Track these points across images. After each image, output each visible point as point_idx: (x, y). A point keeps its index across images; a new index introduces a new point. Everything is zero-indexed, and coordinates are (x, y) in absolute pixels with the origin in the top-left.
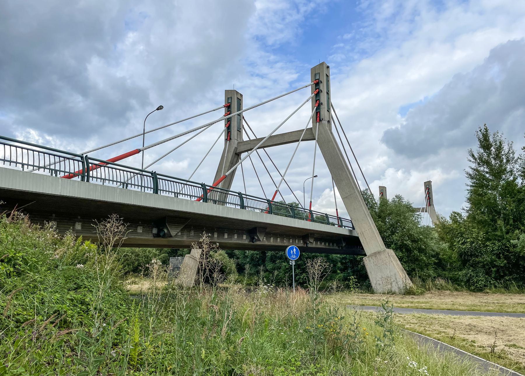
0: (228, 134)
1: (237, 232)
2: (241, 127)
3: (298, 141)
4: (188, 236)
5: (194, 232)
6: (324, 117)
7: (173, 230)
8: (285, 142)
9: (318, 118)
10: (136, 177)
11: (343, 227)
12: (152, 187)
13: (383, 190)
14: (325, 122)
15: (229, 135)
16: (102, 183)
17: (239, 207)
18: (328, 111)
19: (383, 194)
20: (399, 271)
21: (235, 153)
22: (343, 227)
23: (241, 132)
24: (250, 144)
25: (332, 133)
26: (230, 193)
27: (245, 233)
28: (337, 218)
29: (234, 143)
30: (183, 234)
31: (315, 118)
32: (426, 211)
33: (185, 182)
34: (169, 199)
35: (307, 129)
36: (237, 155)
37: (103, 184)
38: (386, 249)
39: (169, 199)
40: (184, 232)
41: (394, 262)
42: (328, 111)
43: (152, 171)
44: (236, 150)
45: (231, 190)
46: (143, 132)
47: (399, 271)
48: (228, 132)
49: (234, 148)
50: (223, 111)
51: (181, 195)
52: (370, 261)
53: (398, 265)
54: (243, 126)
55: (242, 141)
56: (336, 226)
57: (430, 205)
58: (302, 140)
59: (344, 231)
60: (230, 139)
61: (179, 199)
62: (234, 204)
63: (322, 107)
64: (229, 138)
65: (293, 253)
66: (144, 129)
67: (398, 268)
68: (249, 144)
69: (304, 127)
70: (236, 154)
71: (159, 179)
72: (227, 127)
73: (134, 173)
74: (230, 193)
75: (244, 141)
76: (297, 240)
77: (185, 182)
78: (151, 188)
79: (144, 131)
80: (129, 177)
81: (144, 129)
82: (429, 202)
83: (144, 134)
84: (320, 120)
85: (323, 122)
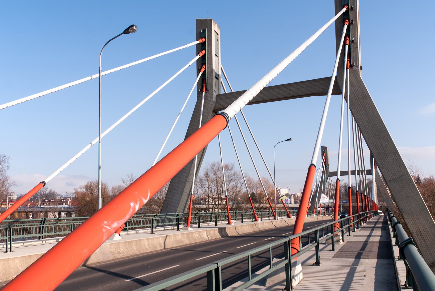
21: (213, 110)
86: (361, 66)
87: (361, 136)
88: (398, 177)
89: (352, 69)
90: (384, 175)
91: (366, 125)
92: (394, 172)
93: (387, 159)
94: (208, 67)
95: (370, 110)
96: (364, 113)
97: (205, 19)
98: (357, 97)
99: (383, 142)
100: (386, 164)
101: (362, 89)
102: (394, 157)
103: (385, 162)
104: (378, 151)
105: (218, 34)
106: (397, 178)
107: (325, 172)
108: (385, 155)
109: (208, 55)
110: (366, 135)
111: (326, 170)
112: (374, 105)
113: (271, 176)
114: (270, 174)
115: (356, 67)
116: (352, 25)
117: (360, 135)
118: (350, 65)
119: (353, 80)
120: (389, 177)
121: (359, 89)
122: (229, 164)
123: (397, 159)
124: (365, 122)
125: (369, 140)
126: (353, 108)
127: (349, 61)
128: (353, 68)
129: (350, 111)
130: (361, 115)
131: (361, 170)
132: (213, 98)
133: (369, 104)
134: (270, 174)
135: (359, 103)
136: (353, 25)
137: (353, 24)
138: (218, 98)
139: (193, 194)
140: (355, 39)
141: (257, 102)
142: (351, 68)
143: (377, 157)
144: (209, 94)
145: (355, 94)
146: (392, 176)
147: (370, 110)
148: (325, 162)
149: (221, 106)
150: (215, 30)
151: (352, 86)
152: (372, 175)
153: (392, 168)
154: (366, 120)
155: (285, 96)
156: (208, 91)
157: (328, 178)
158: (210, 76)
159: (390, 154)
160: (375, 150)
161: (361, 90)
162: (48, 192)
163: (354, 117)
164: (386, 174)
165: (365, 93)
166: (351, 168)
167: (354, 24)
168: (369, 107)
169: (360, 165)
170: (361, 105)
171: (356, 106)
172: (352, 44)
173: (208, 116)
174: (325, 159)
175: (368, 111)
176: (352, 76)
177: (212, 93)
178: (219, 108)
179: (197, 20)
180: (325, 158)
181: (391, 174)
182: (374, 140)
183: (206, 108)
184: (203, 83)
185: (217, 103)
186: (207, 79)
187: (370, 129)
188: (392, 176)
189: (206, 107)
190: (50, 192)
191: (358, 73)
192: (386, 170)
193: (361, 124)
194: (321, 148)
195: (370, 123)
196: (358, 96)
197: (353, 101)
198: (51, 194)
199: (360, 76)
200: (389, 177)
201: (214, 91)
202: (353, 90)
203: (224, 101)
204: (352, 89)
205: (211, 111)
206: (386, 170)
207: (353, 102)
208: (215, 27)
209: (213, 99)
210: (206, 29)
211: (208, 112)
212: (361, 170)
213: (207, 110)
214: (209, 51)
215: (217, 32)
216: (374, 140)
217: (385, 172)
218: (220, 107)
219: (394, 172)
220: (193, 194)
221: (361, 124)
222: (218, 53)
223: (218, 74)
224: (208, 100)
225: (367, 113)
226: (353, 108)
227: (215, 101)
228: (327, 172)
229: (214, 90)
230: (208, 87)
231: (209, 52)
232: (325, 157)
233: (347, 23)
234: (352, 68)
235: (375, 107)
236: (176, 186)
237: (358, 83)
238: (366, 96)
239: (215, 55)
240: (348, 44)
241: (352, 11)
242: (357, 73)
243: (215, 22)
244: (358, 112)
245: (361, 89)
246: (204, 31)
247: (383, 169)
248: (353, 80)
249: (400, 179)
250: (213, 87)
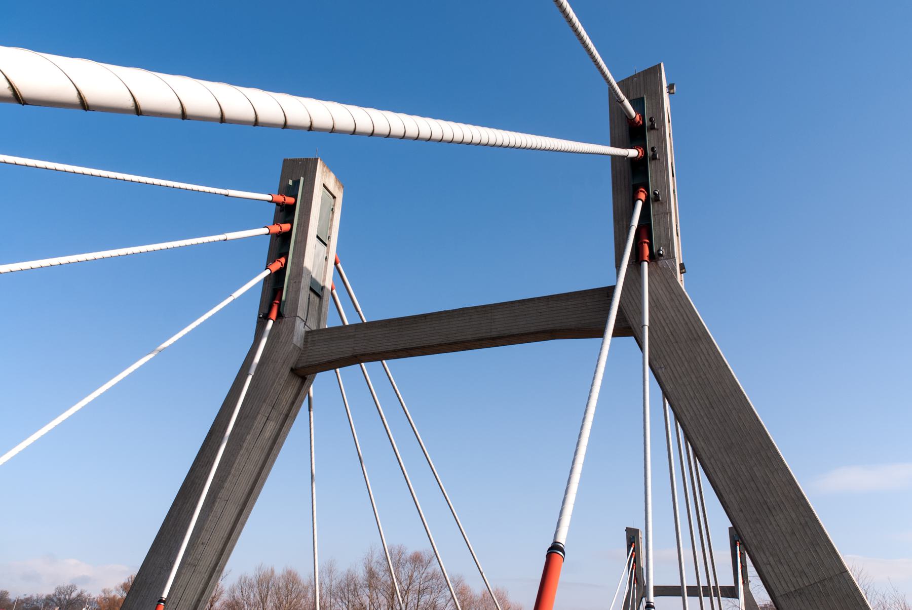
8: (494, 334)
21: (292, 370)
86: (683, 263)
87: (697, 470)
88: (812, 582)
89: (657, 264)
90: (765, 574)
91: (702, 415)
92: (798, 566)
93: (773, 523)
94: (292, 263)
95: (710, 374)
96: (694, 380)
97: (304, 159)
98: (671, 337)
99: (755, 469)
100: (770, 536)
101: (685, 316)
102: (794, 516)
103: (766, 530)
104: (740, 494)
105: (334, 197)
106: (815, 585)
107: (635, 585)
108: (765, 507)
109: (299, 235)
110: (703, 444)
111: (637, 582)
112: (723, 361)
113: (483, 577)
114: (481, 572)
115: (667, 259)
116: (653, 162)
117: (695, 462)
118: (650, 254)
119: (660, 291)
120: (783, 583)
121: (676, 315)
122: (424, 553)
123: (803, 522)
124: (699, 407)
125: (712, 460)
126: (662, 366)
127: (647, 243)
128: (660, 263)
129: (649, 373)
130: (685, 386)
131: (714, 585)
132: (293, 336)
133: (707, 356)
134: (482, 571)
135: (680, 352)
136: (656, 161)
137: (656, 158)
138: (309, 340)
139: (164, 602)
140: (661, 191)
141: (407, 349)
142: (654, 263)
143: (741, 514)
144: (285, 326)
145: (666, 330)
146: (794, 580)
147: (710, 374)
148: (634, 562)
149: (315, 359)
150: (324, 184)
151: (657, 308)
152: (738, 599)
153: (791, 554)
154: (701, 402)
155: (478, 336)
156: (284, 320)
157: (642, 598)
158: (295, 282)
159: (782, 506)
160: (734, 492)
161: (684, 319)
162: (74, 595)
163: (680, 424)
164: (773, 571)
165: (695, 326)
166: (690, 581)
167: (659, 159)
168: (706, 363)
169: (709, 568)
170: (683, 359)
171: (668, 360)
172: (656, 204)
173: (273, 383)
174: (634, 556)
175: (705, 375)
176: (655, 282)
177: (293, 324)
178: (308, 363)
179: (285, 160)
180: (634, 553)
181: (790, 573)
182: (728, 460)
183: (272, 362)
184: (274, 298)
185: (306, 350)
186: (287, 291)
187: (715, 428)
188: (794, 580)
189: (272, 358)
190: (79, 596)
191: (672, 275)
192: (771, 559)
193: (686, 413)
194: (626, 530)
195: (711, 410)
196: (674, 334)
197: (662, 348)
198: (80, 601)
199: (677, 282)
200: (783, 583)
201: (298, 321)
202: (661, 318)
203: (323, 346)
204: (659, 314)
205: (286, 372)
206: (771, 559)
207: (661, 351)
208: (324, 178)
209: (292, 338)
210: (302, 179)
211: (277, 372)
212: (714, 585)
213: (274, 367)
214: (302, 225)
215: (332, 192)
216: (728, 460)
217: (770, 564)
218: (310, 362)
219: (798, 566)
220: (164, 602)
221: (687, 410)
222: (329, 239)
223: (322, 284)
224: (280, 340)
225: (703, 380)
226: (662, 366)
227: (298, 345)
228: (641, 586)
229: (299, 317)
230: (286, 311)
231: (302, 228)
232: (634, 550)
233: (738, 545)
234: (656, 261)
235: (726, 366)
236: (156, 575)
237: (672, 299)
238: (698, 334)
239: (318, 237)
240: (644, 200)
241: (652, 132)
242: (670, 274)
243: (331, 167)
244: (675, 377)
245: (682, 316)
246: (297, 183)
247: (762, 555)
248: (660, 291)
249: (820, 592)
250: (297, 309)
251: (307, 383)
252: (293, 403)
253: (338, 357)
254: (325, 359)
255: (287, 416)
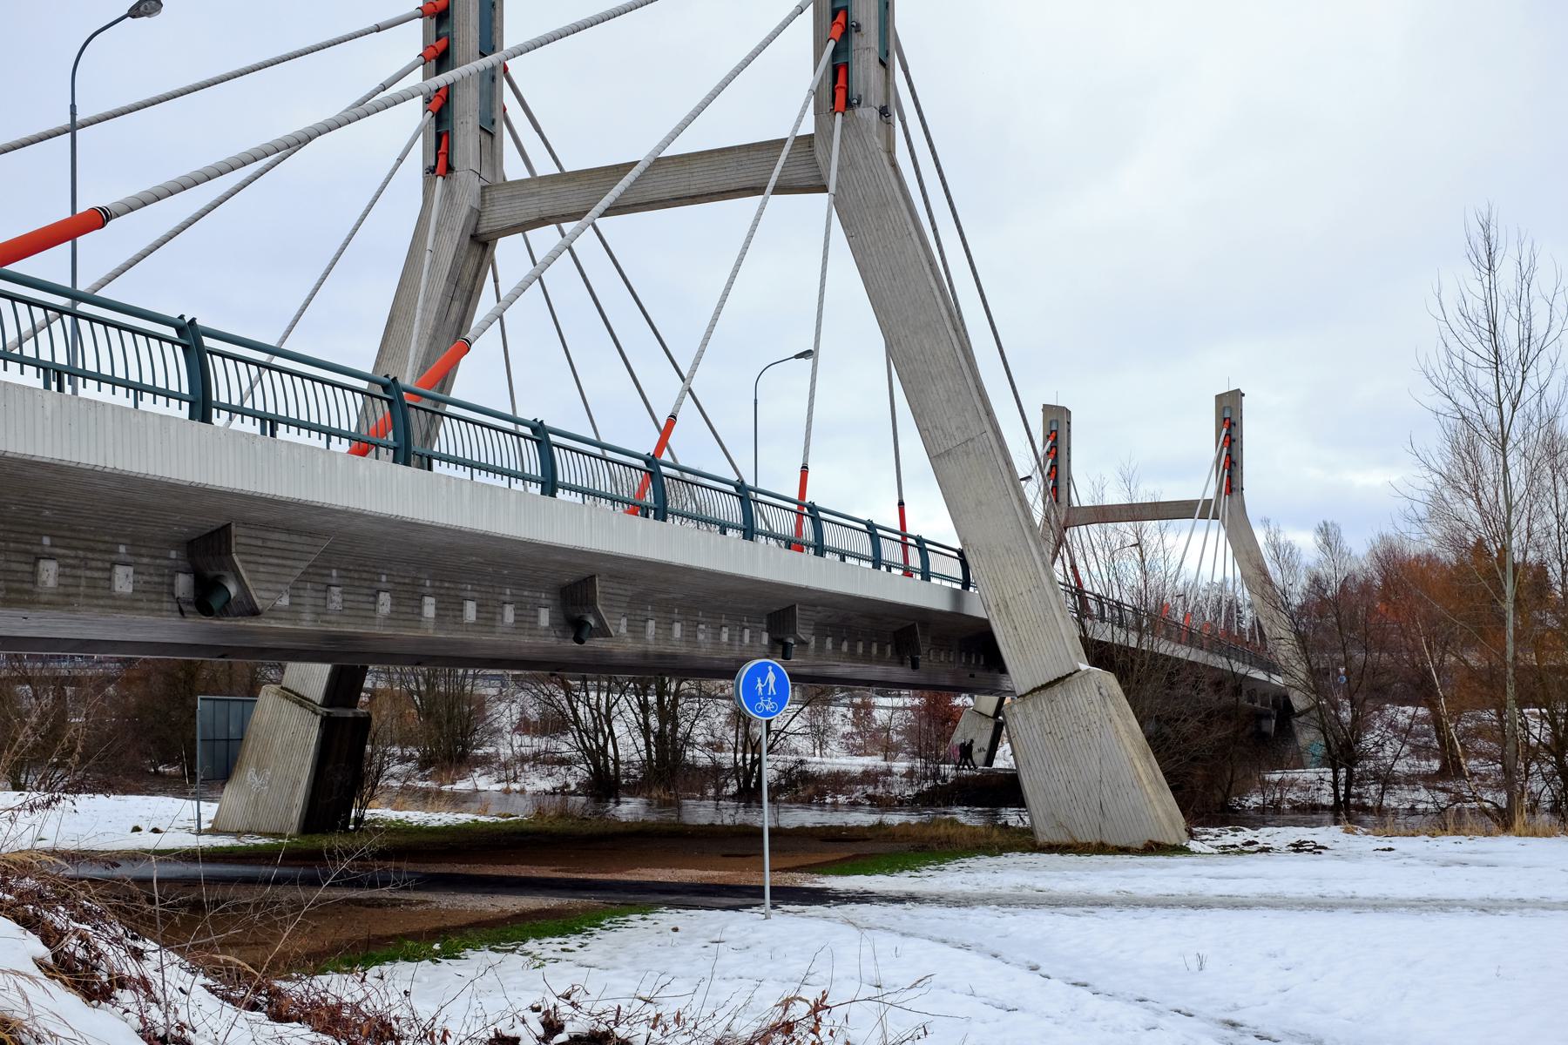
0: (438, 147)
1: (512, 595)
2: (498, 115)
3: (757, 190)
4: (320, 610)
5: (342, 593)
6: (866, 91)
7: (265, 586)
8: (693, 192)
9: (840, 94)
10: (56, 326)
11: (884, 568)
12: (185, 390)
13: (1057, 421)
14: (868, 114)
15: (443, 149)
16: (130, 403)
17: (535, 489)
18: (880, 61)
19: (1056, 437)
20: (1134, 755)
21: (472, 236)
22: (884, 568)
23: (497, 138)
24: (539, 193)
25: (894, 165)
26: (450, 409)
27: (544, 602)
28: (899, 537)
29: (467, 181)
30: (297, 600)
31: (827, 94)
32: (1215, 517)
33: (263, 357)
34: (82, 406)
35: (799, 140)
36: (481, 243)
37: (136, 406)
38: (1084, 666)
39: (82, 406)
40: (302, 593)
41: (1116, 718)
42: (884, 63)
43: (182, 317)
44: (473, 222)
45: (455, 393)
46: (67, 121)
47: (1134, 755)
48: (439, 137)
49: (465, 211)
50: (412, 40)
51: (92, 384)
52: (1027, 717)
53: (1131, 731)
54: (505, 110)
55: (500, 181)
56: (897, 572)
57: (1230, 490)
58: (778, 190)
59: (932, 596)
60: (450, 168)
61: (439, 475)
62: (319, 429)
63: (856, 39)
64: (441, 163)
65: (765, 689)
66: (73, 107)
67: (1133, 745)
68: (533, 195)
69: (782, 130)
70: (475, 238)
71: (213, 352)
72: (436, 109)
73: (46, 307)
74: (450, 409)
75: (508, 179)
76: (747, 632)
77: (263, 357)
78: (180, 397)
79: (73, 113)
80: (26, 326)
81: (73, 107)
82: (1229, 477)
83: (73, 128)
84: (849, 104)
85: (861, 112)
179: (1219, 398)
237: (866, 157)
251: (489, 250)
252: (476, 276)
253: (524, 220)
254: (509, 223)
255: (471, 292)
